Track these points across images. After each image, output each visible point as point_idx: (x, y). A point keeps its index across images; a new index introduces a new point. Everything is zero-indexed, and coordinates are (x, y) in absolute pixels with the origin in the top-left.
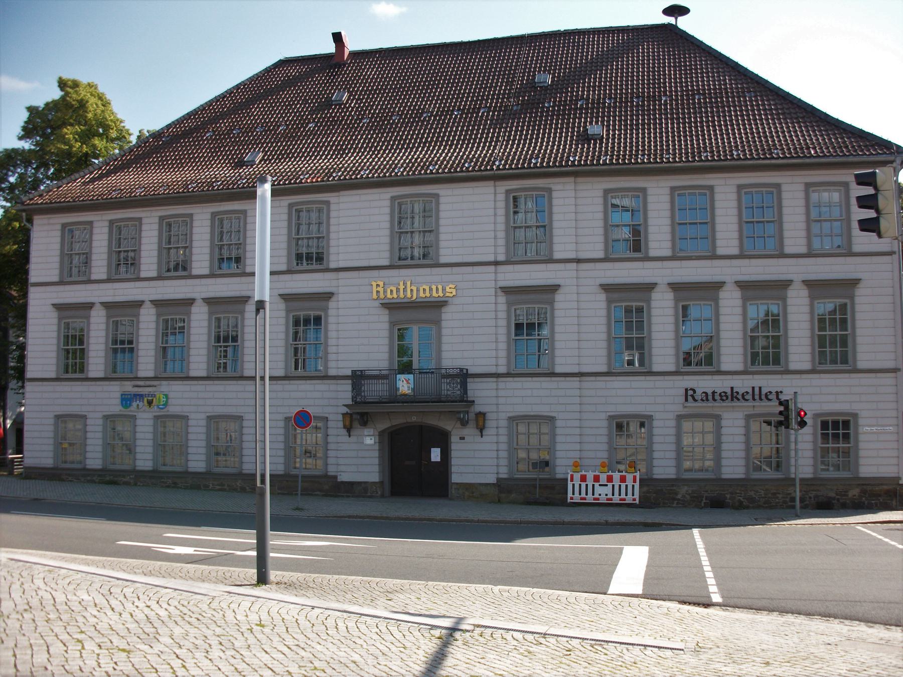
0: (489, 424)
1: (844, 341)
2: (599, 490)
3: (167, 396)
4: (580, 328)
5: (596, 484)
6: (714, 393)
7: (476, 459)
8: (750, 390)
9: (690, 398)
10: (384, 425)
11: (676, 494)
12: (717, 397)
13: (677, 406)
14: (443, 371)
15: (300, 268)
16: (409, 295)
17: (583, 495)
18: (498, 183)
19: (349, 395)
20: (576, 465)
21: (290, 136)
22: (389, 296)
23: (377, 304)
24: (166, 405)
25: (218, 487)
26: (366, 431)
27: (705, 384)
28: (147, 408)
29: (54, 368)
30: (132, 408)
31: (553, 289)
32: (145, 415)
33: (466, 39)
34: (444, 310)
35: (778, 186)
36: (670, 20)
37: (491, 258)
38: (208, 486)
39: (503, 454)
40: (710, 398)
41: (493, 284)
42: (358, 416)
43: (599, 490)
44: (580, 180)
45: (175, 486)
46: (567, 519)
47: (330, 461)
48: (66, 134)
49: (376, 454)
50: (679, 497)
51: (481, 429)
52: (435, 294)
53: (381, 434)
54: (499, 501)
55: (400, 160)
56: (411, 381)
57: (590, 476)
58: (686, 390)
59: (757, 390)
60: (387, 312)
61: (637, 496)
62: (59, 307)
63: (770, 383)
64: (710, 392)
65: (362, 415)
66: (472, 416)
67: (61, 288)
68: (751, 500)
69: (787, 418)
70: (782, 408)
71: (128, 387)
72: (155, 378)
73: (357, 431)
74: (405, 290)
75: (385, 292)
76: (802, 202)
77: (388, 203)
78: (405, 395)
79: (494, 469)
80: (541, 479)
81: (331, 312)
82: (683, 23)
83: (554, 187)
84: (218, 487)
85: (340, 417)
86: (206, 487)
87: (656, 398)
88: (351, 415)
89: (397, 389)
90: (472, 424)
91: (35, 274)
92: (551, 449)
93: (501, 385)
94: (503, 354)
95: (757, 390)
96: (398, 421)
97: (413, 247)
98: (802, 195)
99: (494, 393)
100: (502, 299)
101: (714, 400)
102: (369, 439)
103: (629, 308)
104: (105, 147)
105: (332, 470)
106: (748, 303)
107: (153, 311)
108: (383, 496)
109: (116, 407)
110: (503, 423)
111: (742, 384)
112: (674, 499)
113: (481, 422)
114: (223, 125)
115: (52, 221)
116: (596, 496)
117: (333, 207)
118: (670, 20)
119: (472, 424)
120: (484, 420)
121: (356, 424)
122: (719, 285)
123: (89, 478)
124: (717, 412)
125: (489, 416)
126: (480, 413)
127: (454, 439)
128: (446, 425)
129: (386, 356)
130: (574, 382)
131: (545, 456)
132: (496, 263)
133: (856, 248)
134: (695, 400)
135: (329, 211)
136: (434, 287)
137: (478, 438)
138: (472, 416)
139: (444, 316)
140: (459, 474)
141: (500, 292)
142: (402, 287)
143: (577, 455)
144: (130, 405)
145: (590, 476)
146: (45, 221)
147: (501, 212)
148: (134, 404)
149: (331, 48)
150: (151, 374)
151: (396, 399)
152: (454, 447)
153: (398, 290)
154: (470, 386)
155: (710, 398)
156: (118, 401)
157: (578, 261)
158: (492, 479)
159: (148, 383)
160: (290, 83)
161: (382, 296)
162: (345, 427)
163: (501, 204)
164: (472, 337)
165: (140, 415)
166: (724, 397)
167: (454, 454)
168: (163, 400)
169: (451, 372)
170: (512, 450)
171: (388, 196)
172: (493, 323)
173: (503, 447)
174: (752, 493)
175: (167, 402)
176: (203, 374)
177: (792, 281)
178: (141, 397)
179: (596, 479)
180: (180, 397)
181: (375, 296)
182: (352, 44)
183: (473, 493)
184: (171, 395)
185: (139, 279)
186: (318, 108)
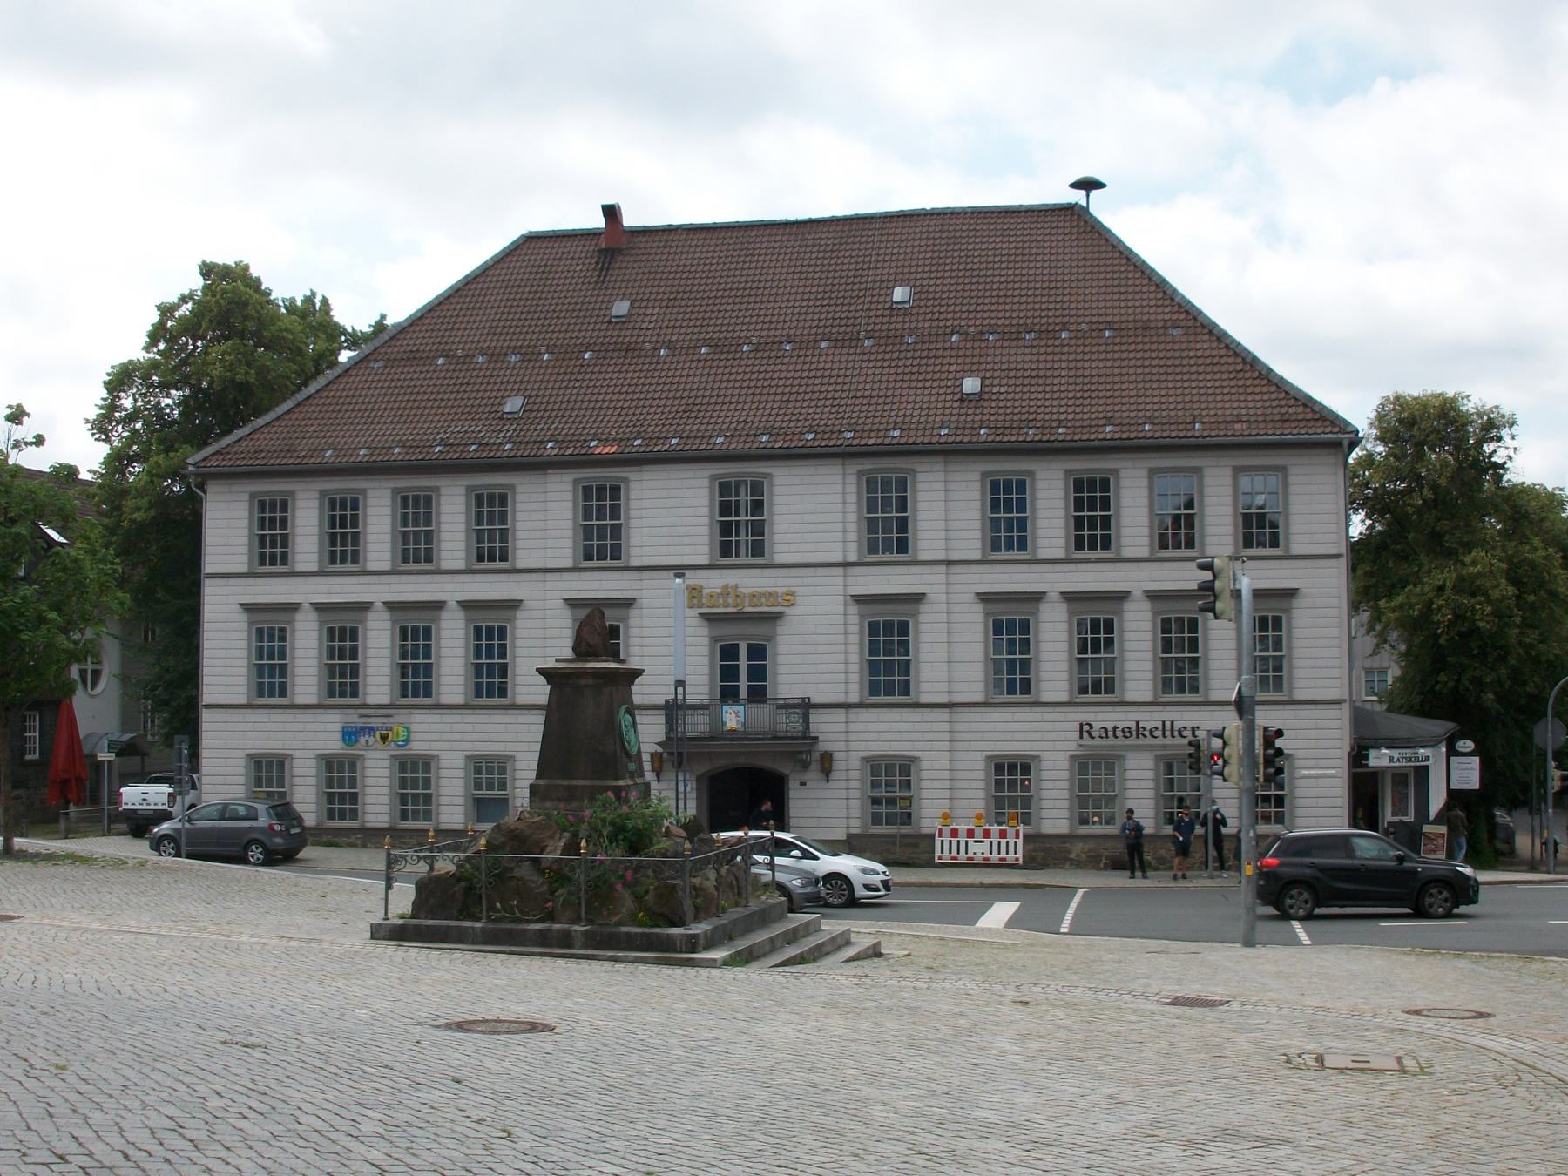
0: (836, 765)
3: (408, 729)
4: (951, 651)
5: (971, 841)
6: (1115, 728)
8: (1160, 725)
10: (703, 768)
12: (1119, 733)
18: (848, 461)
19: (662, 729)
20: (945, 816)
24: (407, 741)
28: (380, 745)
31: (918, 598)
32: (378, 754)
33: (792, 218)
36: (1078, 197)
37: (838, 558)
40: (1110, 734)
46: (935, 880)
50: (1073, 856)
53: (699, 779)
56: (742, 714)
59: (1168, 725)
61: (1020, 855)
63: (1185, 718)
64: (1110, 726)
66: (816, 756)
67: (251, 581)
69: (1198, 759)
70: (1192, 750)
71: (353, 718)
76: (1230, 490)
79: (843, 823)
80: (903, 836)
81: (632, 622)
82: (1101, 207)
87: (1048, 735)
89: (723, 724)
90: (815, 766)
91: (210, 563)
93: (852, 717)
95: (1168, 725)
98: (1229, 481)
103: (1010, 626)
109: (335, 745)
110: (856, 764)
111: (1150, 719)
112: (1067, 859)
113: (826, 763)
118: (1078, 197)
119: (815, 766)
121: (667, 766)
125: (836, 756)
128: (782, 768)
132: (845, 565)
137: (823, 784)
138: (816, 756)
144: (356, 741)
148: (362, 740)
149: (599, 222)
150: (386, 700)
151: (718, 735)
155: (1110, 734)
156: (338, 735)
166: (1127, 732)
168: (403, 734)
172: (843, 813)
178: (371, 730)
180: (428, 732)
184: (414, 727)
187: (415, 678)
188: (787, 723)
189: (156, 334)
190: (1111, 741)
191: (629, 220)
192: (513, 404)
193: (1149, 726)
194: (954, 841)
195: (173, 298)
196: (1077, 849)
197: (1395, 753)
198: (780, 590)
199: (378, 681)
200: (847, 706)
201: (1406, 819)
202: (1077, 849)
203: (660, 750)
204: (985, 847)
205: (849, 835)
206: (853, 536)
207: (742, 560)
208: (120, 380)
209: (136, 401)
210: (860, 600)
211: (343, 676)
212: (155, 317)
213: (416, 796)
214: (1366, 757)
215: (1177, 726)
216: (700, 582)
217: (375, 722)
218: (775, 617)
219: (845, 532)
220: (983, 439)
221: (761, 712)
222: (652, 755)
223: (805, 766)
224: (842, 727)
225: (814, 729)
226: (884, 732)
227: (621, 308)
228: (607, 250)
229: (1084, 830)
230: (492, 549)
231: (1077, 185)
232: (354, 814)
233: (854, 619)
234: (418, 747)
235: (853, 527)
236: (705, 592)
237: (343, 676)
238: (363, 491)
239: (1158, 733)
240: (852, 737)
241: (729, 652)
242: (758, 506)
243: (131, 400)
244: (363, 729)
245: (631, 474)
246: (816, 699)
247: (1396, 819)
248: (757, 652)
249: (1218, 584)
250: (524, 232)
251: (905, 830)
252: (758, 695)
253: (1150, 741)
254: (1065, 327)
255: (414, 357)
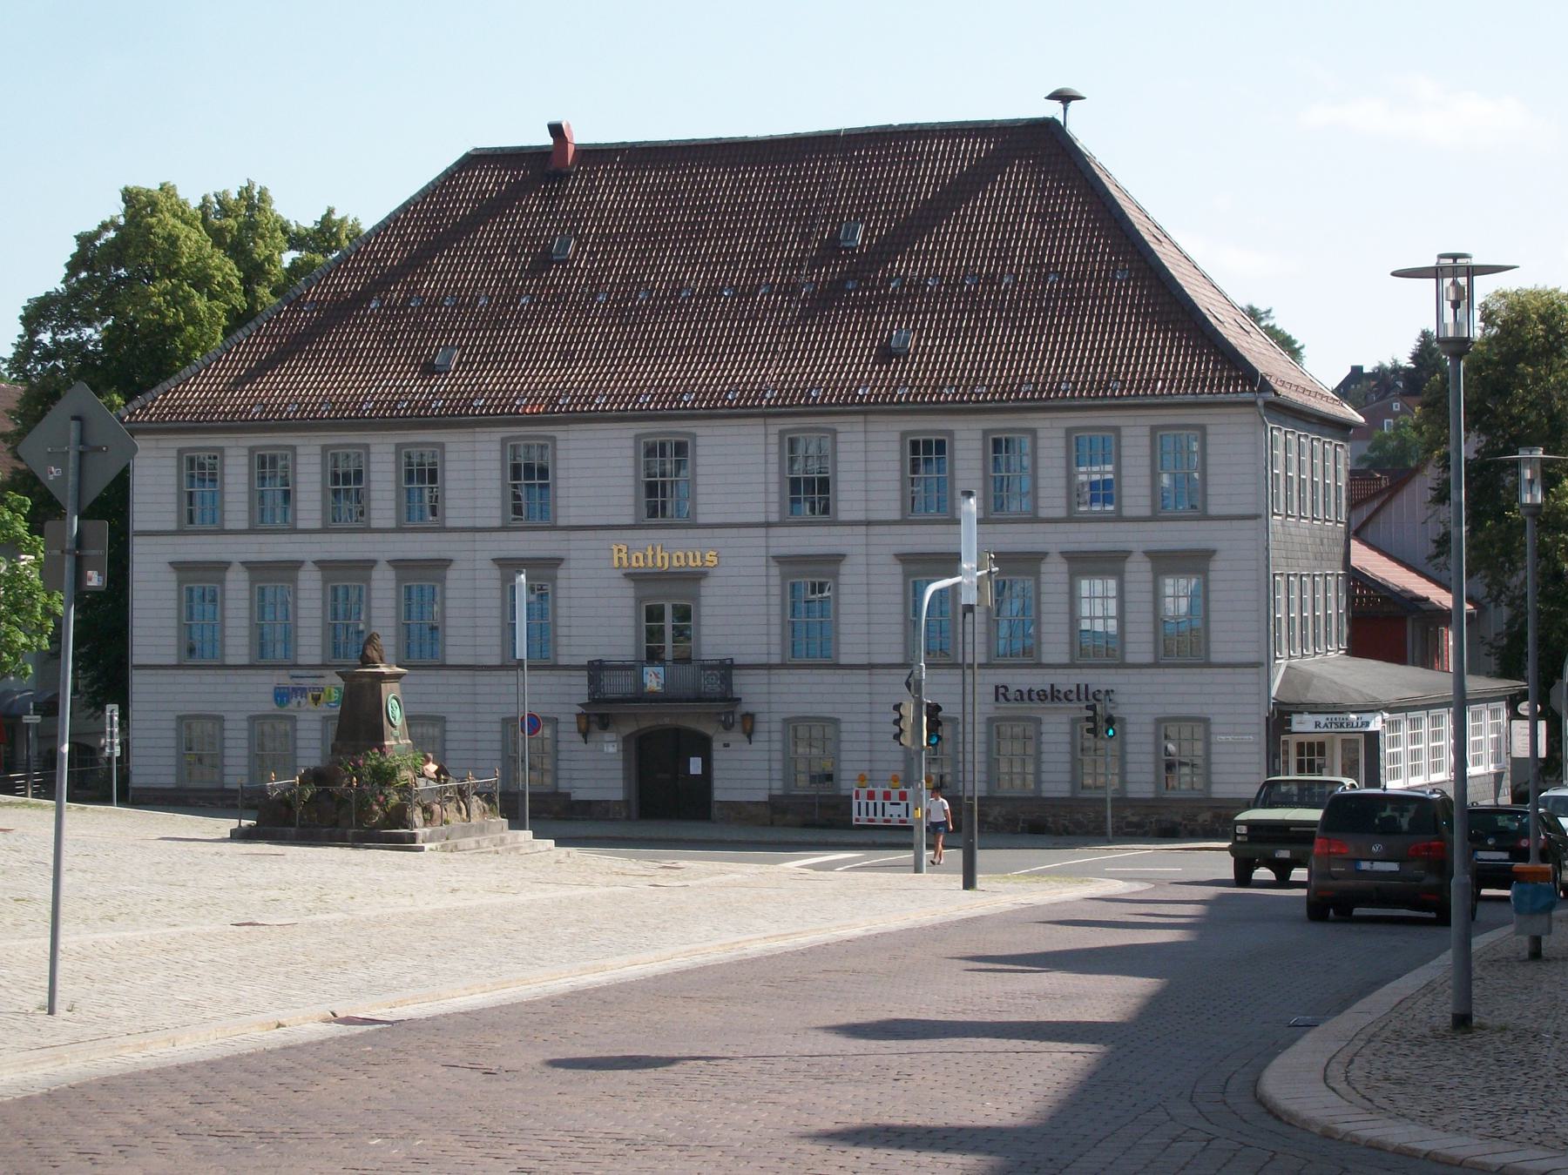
0: (760, 727)
2: (889, 809)
5: (887, 803)
6: (1030, 691)
7: (742, 771)
8: (1074, 689)
10: (629, 728)
12: (1034, 696)
13: (985, 706)
15: (518, 524)
16: (659, 564)
17: (871, 816)
18: (770, 421)
19: (586, 690)
20: (862, 778)
21: (496, 322)
22: (634, 564)
23: (619, 573)
26: (608, 736)
28: (312, 707)
29: (174, 651)
30: (290, 706)
34: (703, 583)
35: (1117, 430)
37: (761, 518)
39: (777, 766)
41: (763, 551)
43: (889, 809)
44: (870, 418)
47: (561, 774)
48: (153, 295)
49: (620, 765)
50: (990, 819)
51: (749, 734)
52: (691, 563)
53: (626, 740)
54: (772, 824)
55: (650, 376)
56: (662, 676)
57: (879, 791)
58: (997, 688)
59: (1083, 688)
62: (179, 567)
65: (602, 716)
66: (737, 717)
70: (1090, 713)
72: (323, 666)
73: (596, 735)
74: (654, 556)
75: (629, 559)
77: (631, 443)
78: (653, 692)
79: (766, 784)
81: (561, 583)
82: (1082, 128)
83: (839, 428)
85: (574, 719)
88: (588, 715)
89: (644, 685)
90: (738, 727)
91: (141, 517)
92: (837, 759)
93: (774, 679)
94: (776, 639)
95: (1083, 688)
96: (645, 724)
99: (765, 689)
100: (775, 570)
101: (1031, 699)
102: (610, 746)
104: (209, 308)
105: (563, 786)
107: (317, 575)
108: (628, 818)
109: (268, 706)
110: (777, 726)
111: (1066, 680)
113: (749, 725)
114: (396, 294)
115: (162, 444)
116: (887, 817)
117: (560, 445)
118: (1054, 110)
119: (738, 727)
120: (753, 723)
121: (594, 727)
124: (1034, 714)
125: (759, 717)
126: (747, 714)
127: (717, 746)
129: (631, 641)
130: (862, 676)
131: (828, 766)
132: (768, 525)
133: (1213, 510)
135: (554, 448)
136: (691, 555)
137: (746, 746)
138: (737, 717)
139: (703, 592)
140: (722, 792)
141: (772, 563)
142: (650, 553)
143: (866, 766)
145: (879, 791)
146: (153, 444)
147: (774, 458)
148: (294, 701)
149: (547, 140)
150: (317, 660)
151: (642, 697)
152: (716, 755)
153: (645, 557)
154: (735, 680)
156: (271, 697)
158: (762, 796)
159: (313, 673)
160: (490, 209)
161: (625, 563)
162: (580, 731)
163: (774, 449)
164: (738, 619)
166: (1042, 696)
167: (715, 765)
170: (789, 762)
171: (632, 433)
173: (778, 755)
174: (1080, 816)
176: (245, 661)
177: (1130, 552)
178: (301, 691)
179: (887, 796)
181: (616, 564)
182: (580, 135)
189: (74, 266)
193: (1063, 689)
194: (871, 803)
195: (92, 227)
200: (768, 667)
204: (901, 809)
205: (771, 796)
206: (774, 498)
208: (37, 313)
209: (55, 334)
210: (782, 560)
212: (74, 248)
214: (1289, 723)
215: (1092, 689)
217: (307, 683)
219: (766, 492)
221: (686, 673)
225: (738, 690)
226: (802, 693)
231: (1055, 96)
233: (776, 581)
235: (774, 488)
238: (221, 450)
241: (654, 614)
243: (49, 334)
245: (558, 432)
246: (738, 660)
248: (684, 614)
250: (468, 148)
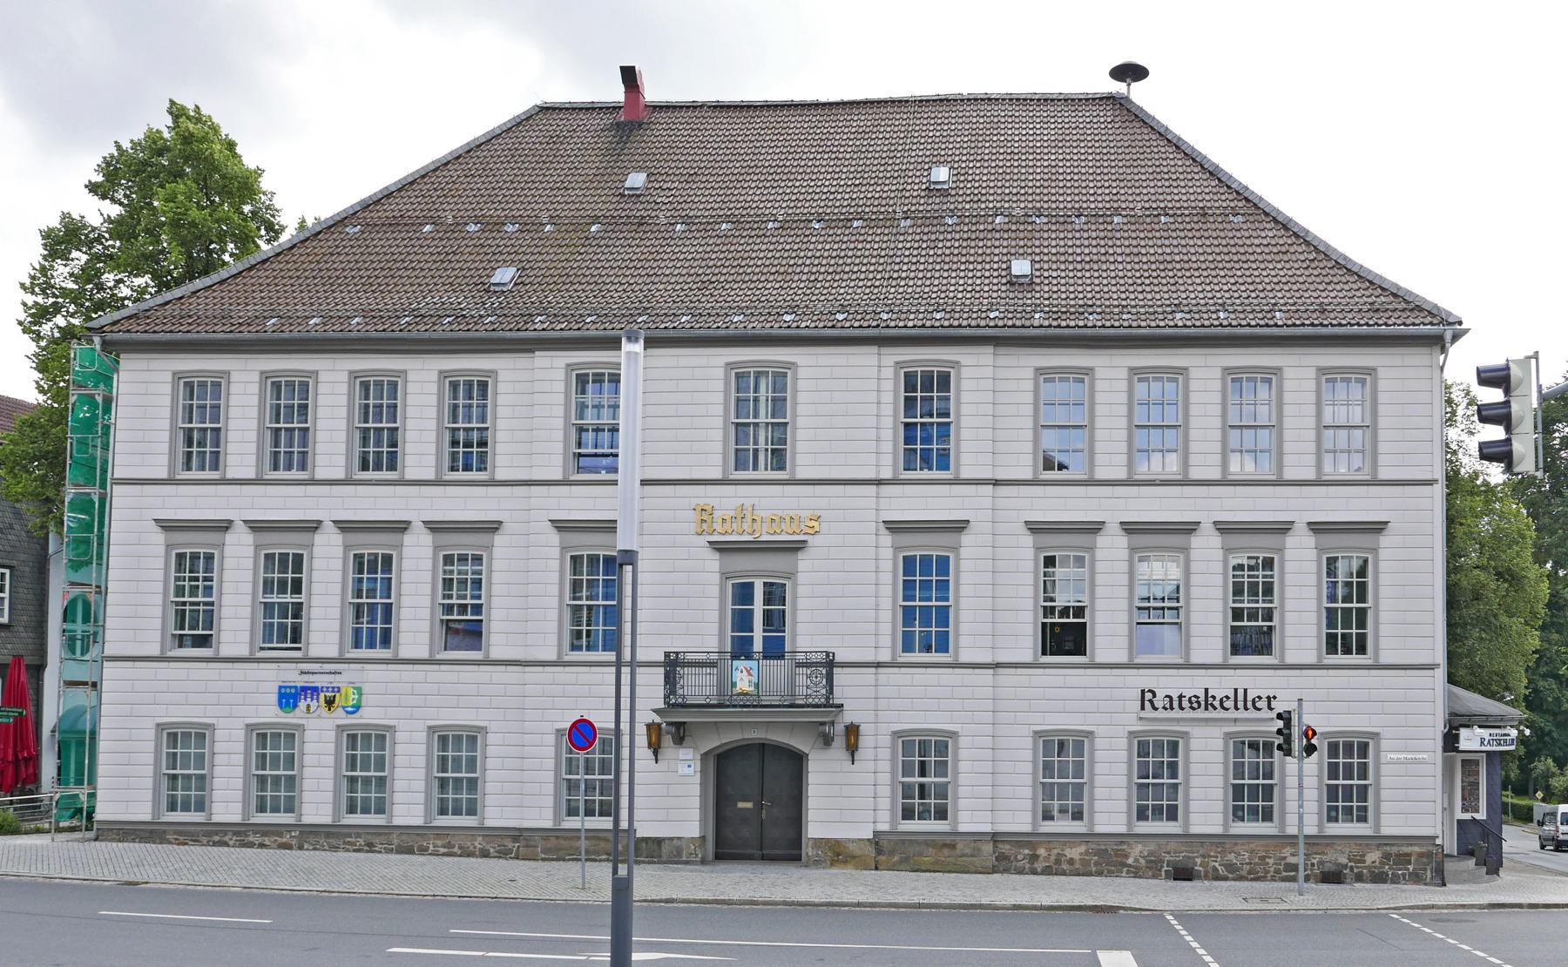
1: (943, 615)
3: (360, 692)
4: (995, 602)
6: (1181, 697)
7: (845, 799)
8: (1232, 695)
9: (1147, 704)
10: (712, 742)
11: (1127, 856)
12: (1185, 703)
13: (1130, 719)
14: (801, 657)
18: (884, 350)
19: (660, 692)
24: (357, 708)
25: (443, 850)
27: (1168, 684)
28: (324, 711)
36: (1118, 87)
38: (426, 849)
40: (1176, 704)
42: (672, 730)
45: (370, 847)
50: (1130, 861)
51: (852, 749)
56: (754, 672)
58: (1143, 692)
60: (717, 555)
65: (679, 725)
66: (840, 728)
68: (1230, 867)
69: (1288, 739)
70: (1280, 724)
71: (292, 676)
84: (443, 850)
86: (423, 851)
89: (734, 685)
90: (839, 742)
91: (123, 463)
97: (760, 443)
106: (1136, 556)
108: (703, 862)
109: (270, 713)
110: (886, 740)
111: (1222, 685)
112: (1125, 865)
118: (1118, 87)
121: (667, 741)
122: (1190, 528)
123: (216, 838)
130: (986, 676)
134: (1156, 709)
144: (295, 706)
148: (302, 705)
151: (726, 701)
155: (1176, 704)
156: (274, 698)
157: (996, 483)
159: (328, 667)
162: (650, 746)
165: (311, 723)
166: (1195, 704)
169: (814, 658)
175: (359, 700)
178: (315, 690)
183: (837, 854)
184: (366, 688)
185: (313, 482)
186: (595, 218)
187: (373, 625)
188: (807, 686)
190: (1176, 713)
191: (652, 93)
192: (504, 275)
196: (1136, 852)
197: (1485, 733)
198: (805, 514)
199: (326, 623)
201: (1478, 816)
202: (1136, 852)
203: (658, 719)
205: (876, 833)
207: (761, 474)
211: (284, 626)
213: (277, 779)
216: (712, 502)
217: (318, 681)
218: (796, 548)
220: (1036, 323)
221: (776, 670)
222: (649, 726)
223: (827, 741)
224: (871, 692)
225: (839, 696)
227: (637, 180)
228: (625, 124)
229: (1144, 827)
230: (468, 451)
232: (201, 806)
234: (370, 715)
236: (717, 514)
237: (284, 626)
238: (494, 373)
239: (1229, 704)
240: (882, 703)
241: (744, 593)
242: (778, 405)
244: (304, 689)
247: (1467, 816)
248: (775, 594)
249: (1515, 407)
251: (198, 817)
252: (775, 650)
253: (1220, 714)
254: (1117, 211)
255: (394, 224)
